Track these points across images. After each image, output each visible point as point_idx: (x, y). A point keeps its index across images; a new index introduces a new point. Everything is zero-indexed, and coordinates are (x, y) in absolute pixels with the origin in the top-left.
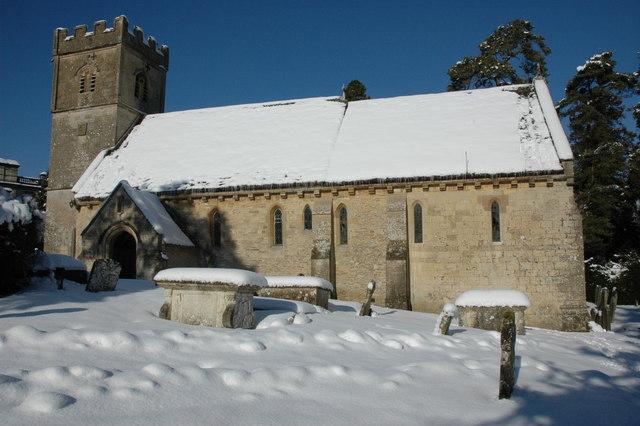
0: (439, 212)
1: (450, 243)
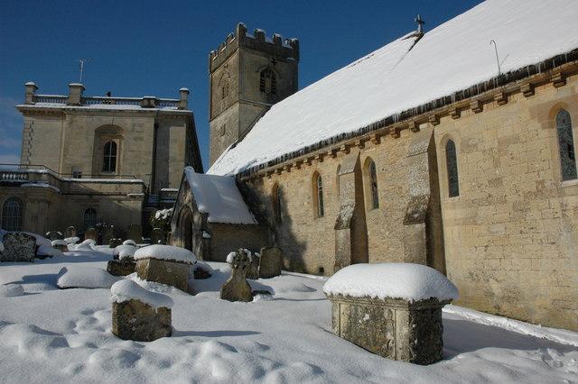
0: (475, 145)
1: (493, 191)
